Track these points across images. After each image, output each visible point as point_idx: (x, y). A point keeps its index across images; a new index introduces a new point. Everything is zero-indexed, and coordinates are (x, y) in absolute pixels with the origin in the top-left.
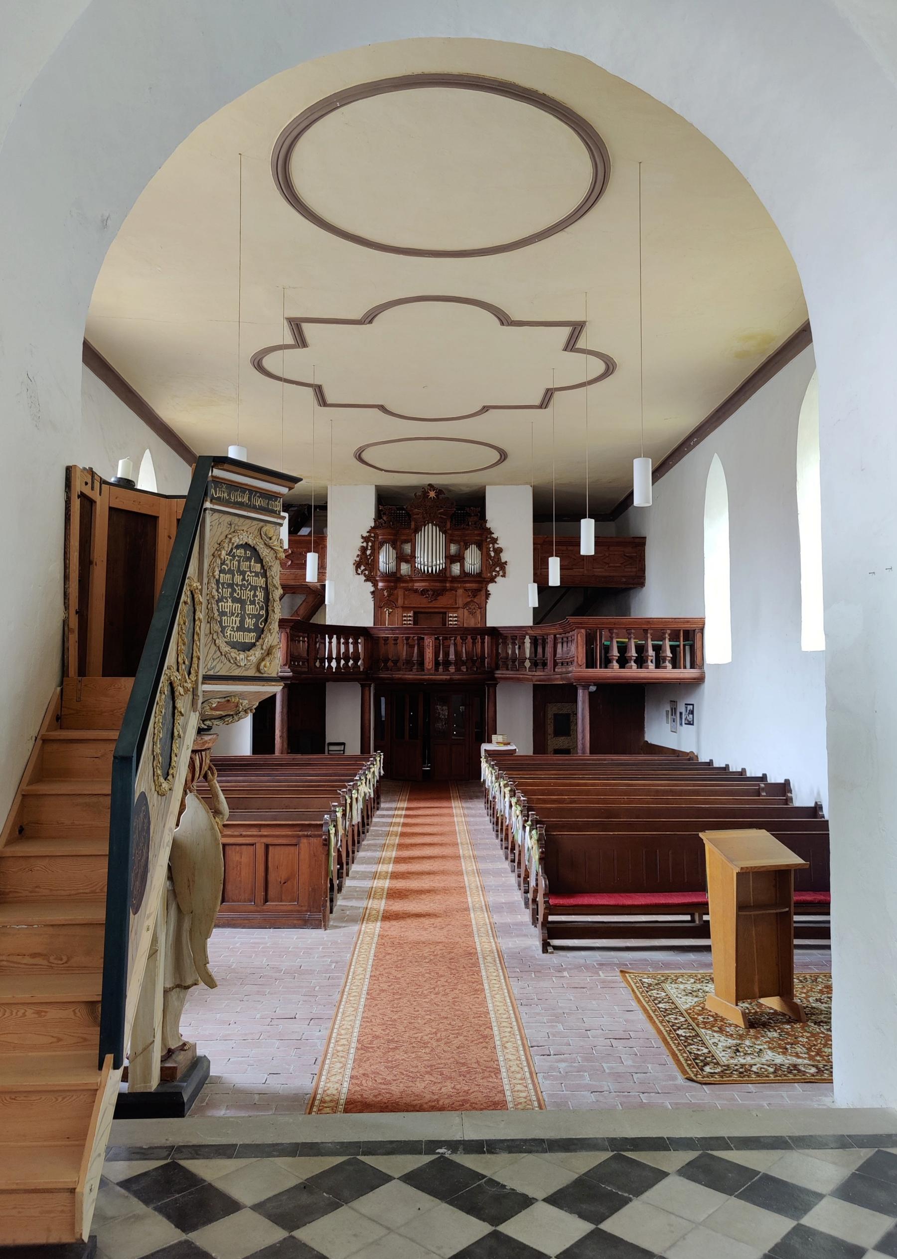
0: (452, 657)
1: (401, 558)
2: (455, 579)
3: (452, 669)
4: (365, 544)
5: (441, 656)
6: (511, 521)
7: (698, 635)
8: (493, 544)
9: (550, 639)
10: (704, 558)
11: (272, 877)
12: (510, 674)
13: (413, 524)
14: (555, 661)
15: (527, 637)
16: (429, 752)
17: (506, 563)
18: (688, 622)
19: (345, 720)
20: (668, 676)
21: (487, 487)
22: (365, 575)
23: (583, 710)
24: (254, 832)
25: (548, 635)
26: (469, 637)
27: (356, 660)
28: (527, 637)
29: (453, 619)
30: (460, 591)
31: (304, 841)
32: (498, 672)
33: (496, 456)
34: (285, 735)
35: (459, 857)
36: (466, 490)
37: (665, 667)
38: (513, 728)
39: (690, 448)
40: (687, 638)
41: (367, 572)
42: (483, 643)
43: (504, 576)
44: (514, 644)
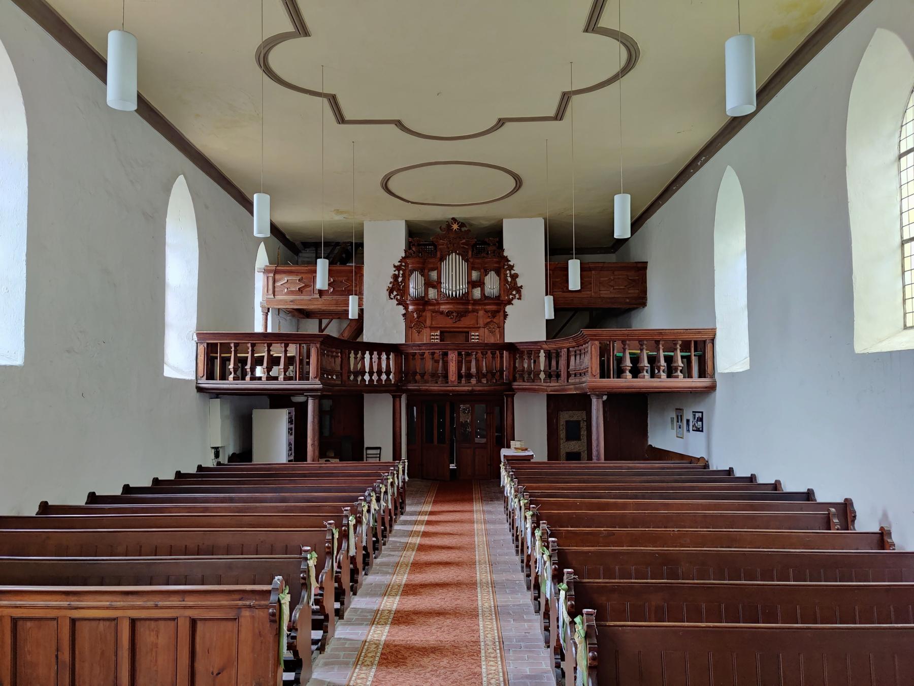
0: (473, 370)
1: (429, 284)
2: (476, 302)
3: (473, 381)
4: (397, 273)
6: (525, 249)
7: (709, 346)
9: (564, 352)
10: (714, 271)
11: (199, 666)
12: (527, 385)
13: (438, 254)
14: (568, 372)
15: (542, 351)
16: (453, 455)
17: (521, 287)
18: (699, 333)
19: (380, 425)
20: (680, 385)
21: (505, 221)
23: (597, 418)
24: (175, 602)
25: (561, 348)
26: (489, 352)
27: (388, 373)
28: (542, 351)
29: (475, 337)
30: (481, 313)
31: (246, 613)
32: (515, 383)
33: (512, 183)
34: (316, 443)
35: (475, 584)
36: (486, 223)
37: (677, 377)
38: (529, 436)
39: (697, 169)
40: (698, 349)
42: (502, 357)
43: (520, 299)
44: (529, 358)
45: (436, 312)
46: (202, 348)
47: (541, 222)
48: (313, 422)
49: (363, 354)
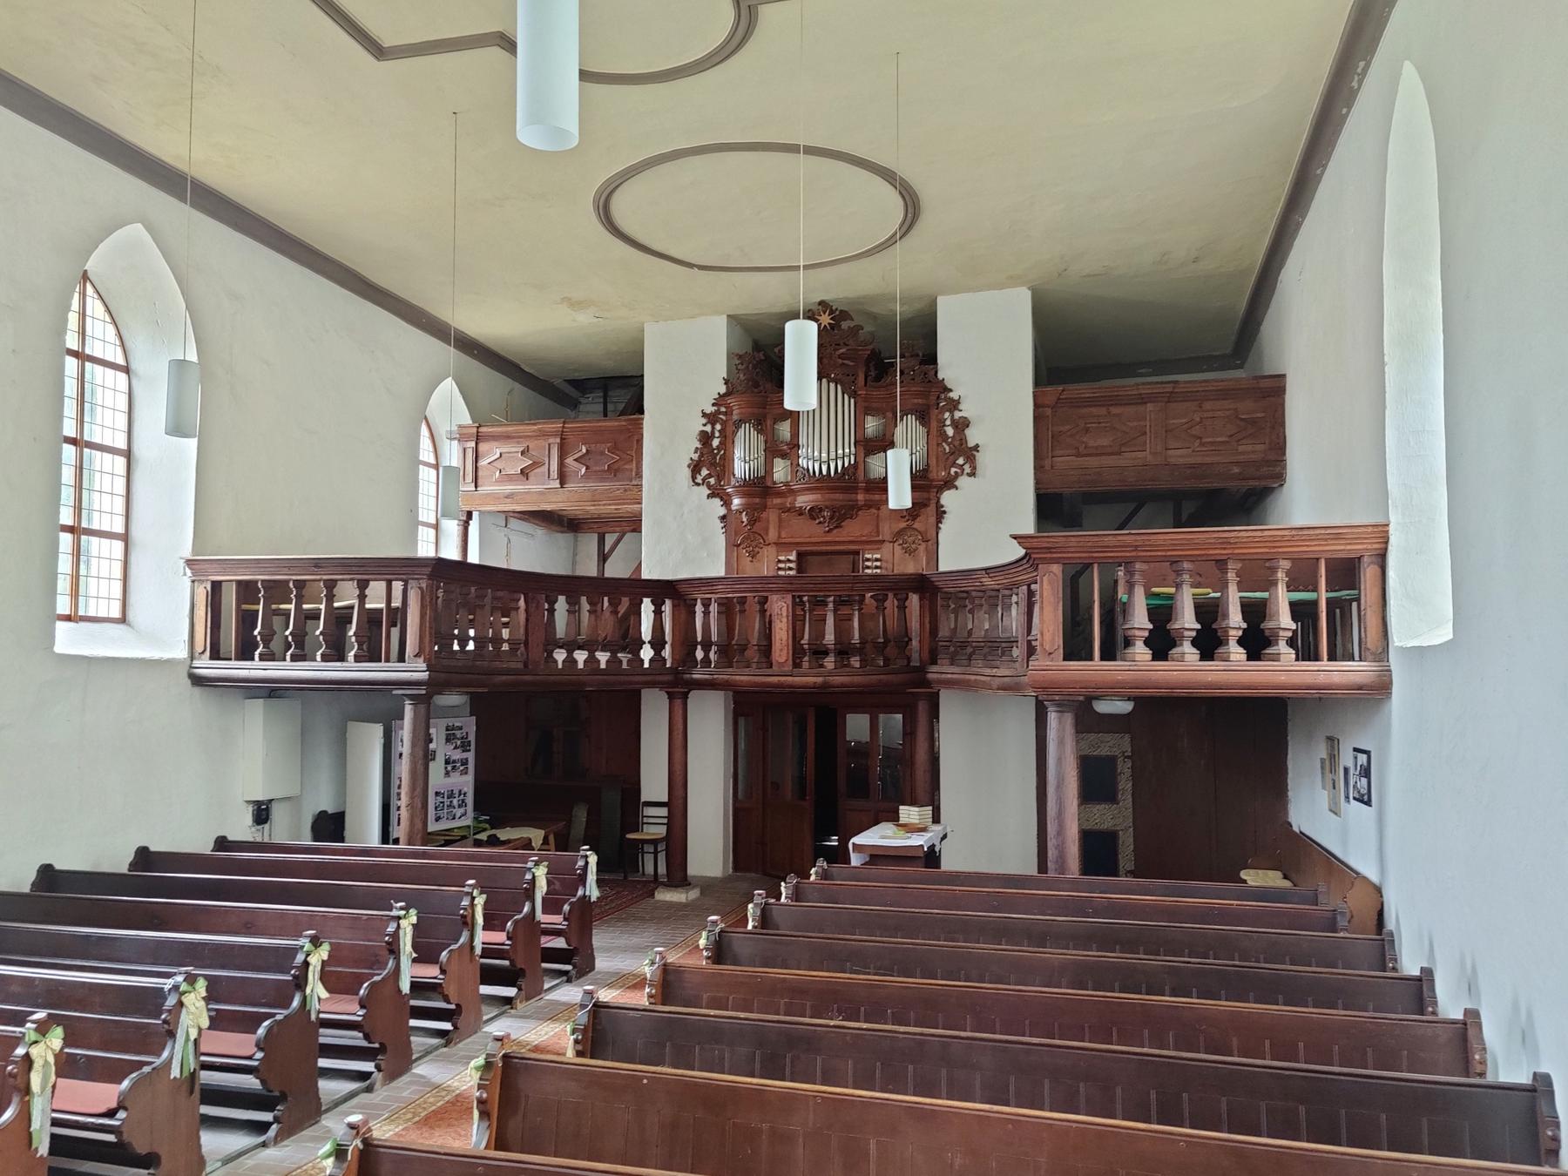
0: (830, 638)
1: (774, 450)
3: (829, 662)
4: (708, 428)
5: (806, 636)
6: (990, 369)
7: (1368, 574)
8: (952, 412)
18: (1338, 537)
20: (1283, 678)
21: (942, 303)
22: (709, 487)
23: (1060, 760)
32: (934, 668)
37: (1276, 658)
41: (712, 481)
43: (972, 474)
45: (789, 510)
47: (1020, 303)
49: (552, 602)
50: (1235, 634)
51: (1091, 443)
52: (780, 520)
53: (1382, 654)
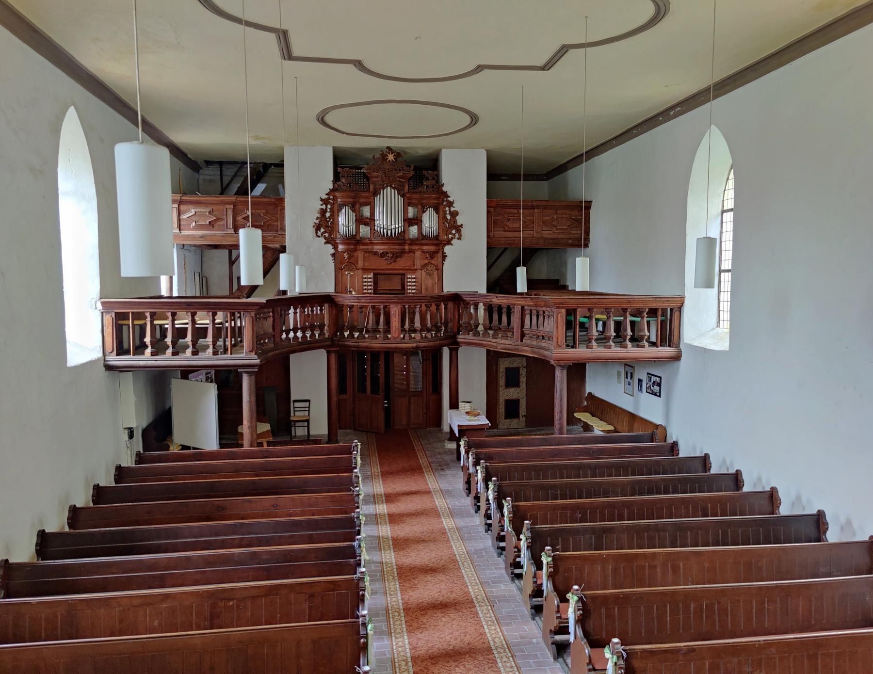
0: (417, 324)
1: (360, 221)
2: (413, 242)
4: (324, 207)
6: (465, 184)
7: (676, 314)
13: (371, 186)
14: (522, 332)
16: (388, 409)
21: (443, 151)
22: (325, 238)
23: (561, 390)
26: (433, 304)
30: (418, 254)
33: (467, 120)
35: (489, 650)
36: (422, 152)
37: (643, 347)
41: (327, 235)
43: (459, 238)
46: (109, 319)
48: (250, 402)
50: (629, 337)
51: (511, 226)
52: (364, 257)
53: (678, 346)
